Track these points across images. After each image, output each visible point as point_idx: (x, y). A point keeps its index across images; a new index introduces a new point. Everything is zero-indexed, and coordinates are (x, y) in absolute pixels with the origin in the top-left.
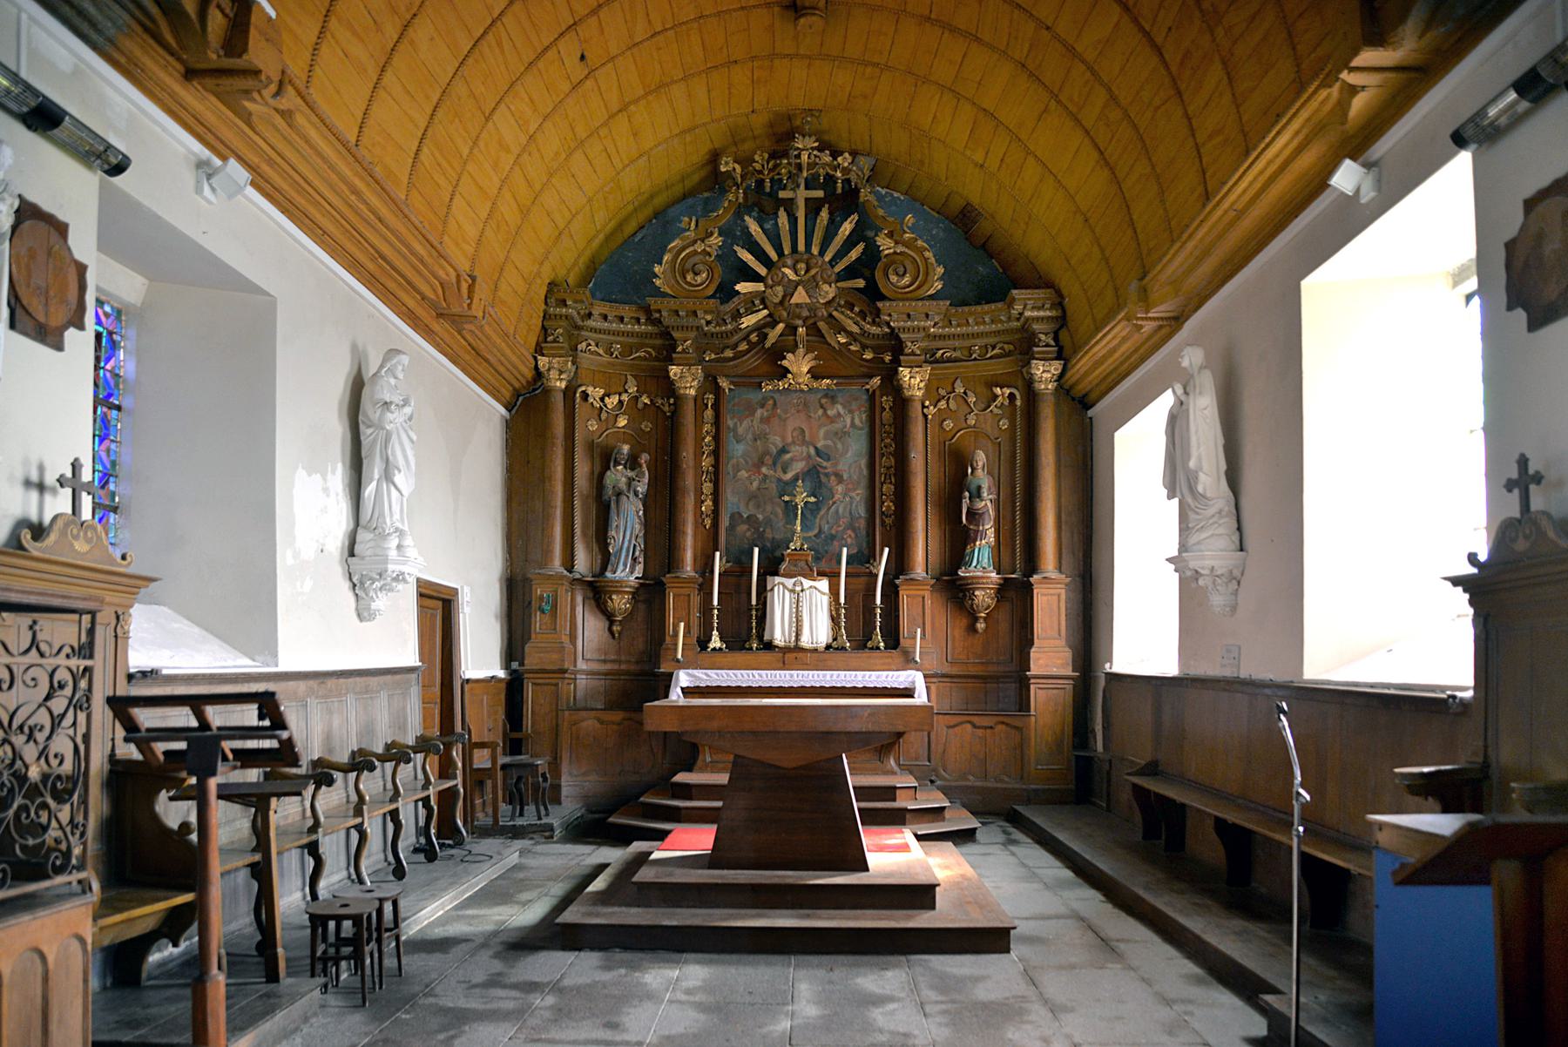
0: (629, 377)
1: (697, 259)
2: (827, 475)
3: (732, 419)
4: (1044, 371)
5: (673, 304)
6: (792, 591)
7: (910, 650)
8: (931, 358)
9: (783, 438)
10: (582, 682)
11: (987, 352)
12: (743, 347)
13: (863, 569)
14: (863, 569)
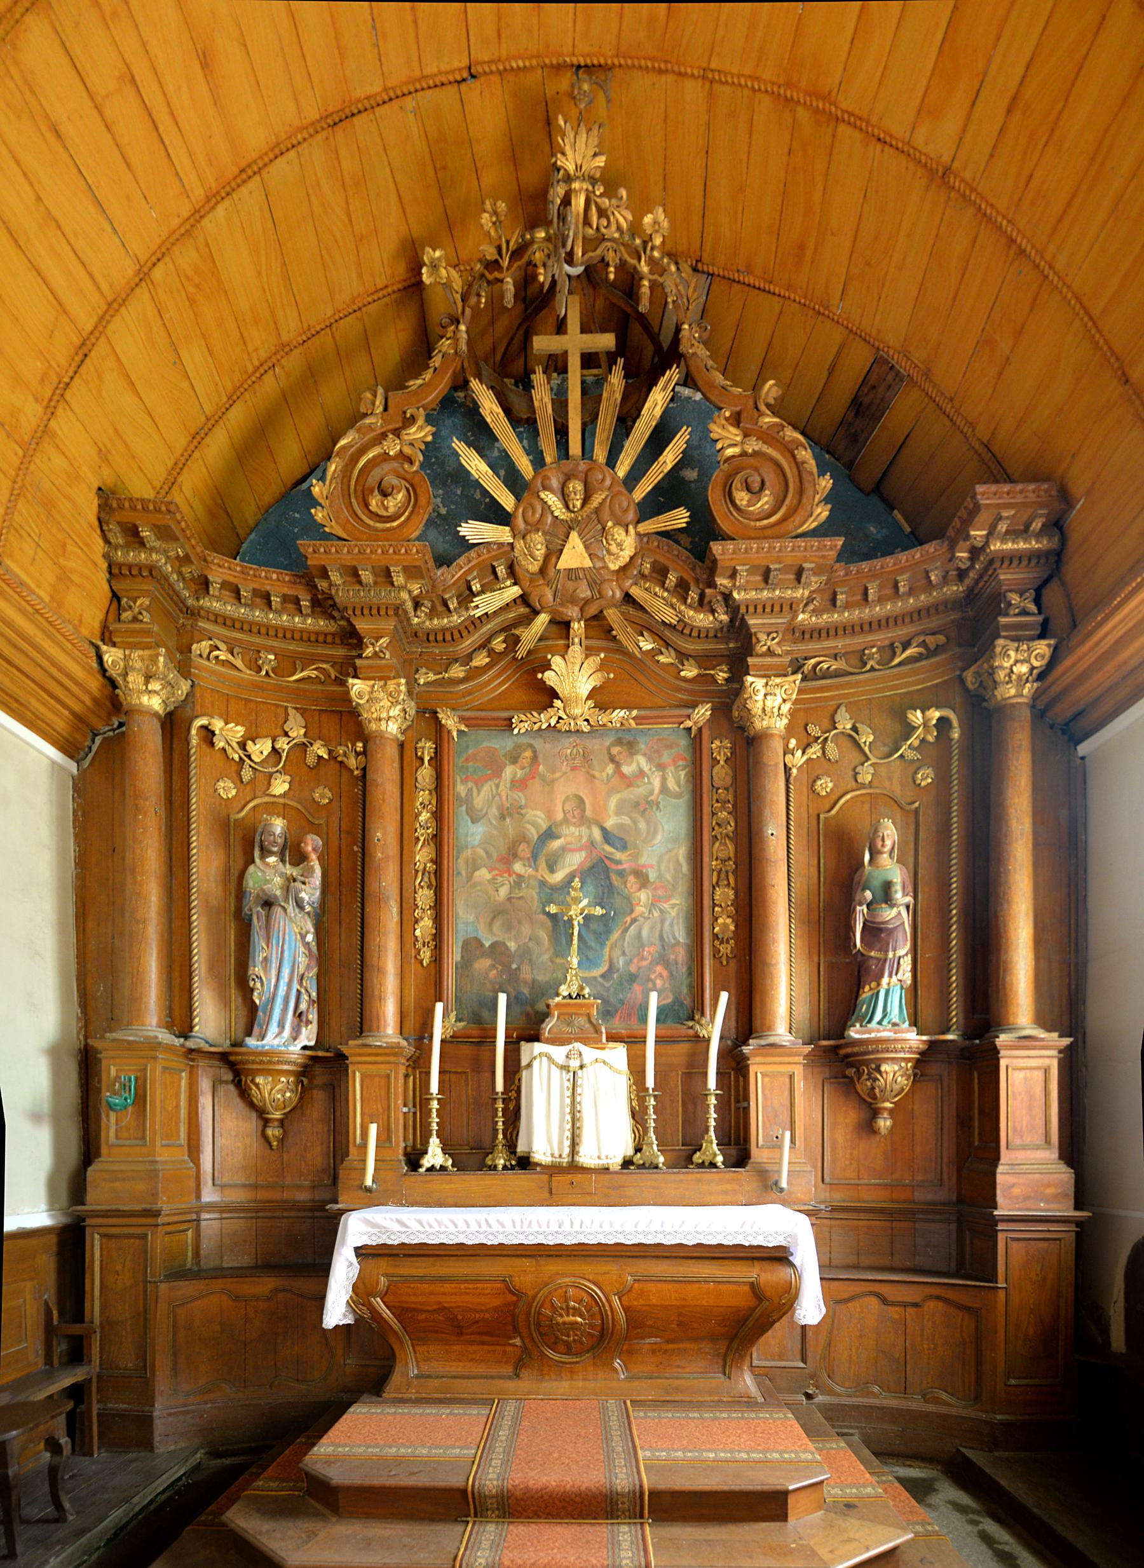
0: (291, 711)
1: (387, 467)
2: (621, 874)
3: (465, 781)
4: (1016, 662)
5: (345, 554)
6: (565, 1068)
7: (769, 1167)
9: (549, 814)
10: (210, 1224)
12: (481, 660)
13: (683, 1030)
14: (683, 1030)
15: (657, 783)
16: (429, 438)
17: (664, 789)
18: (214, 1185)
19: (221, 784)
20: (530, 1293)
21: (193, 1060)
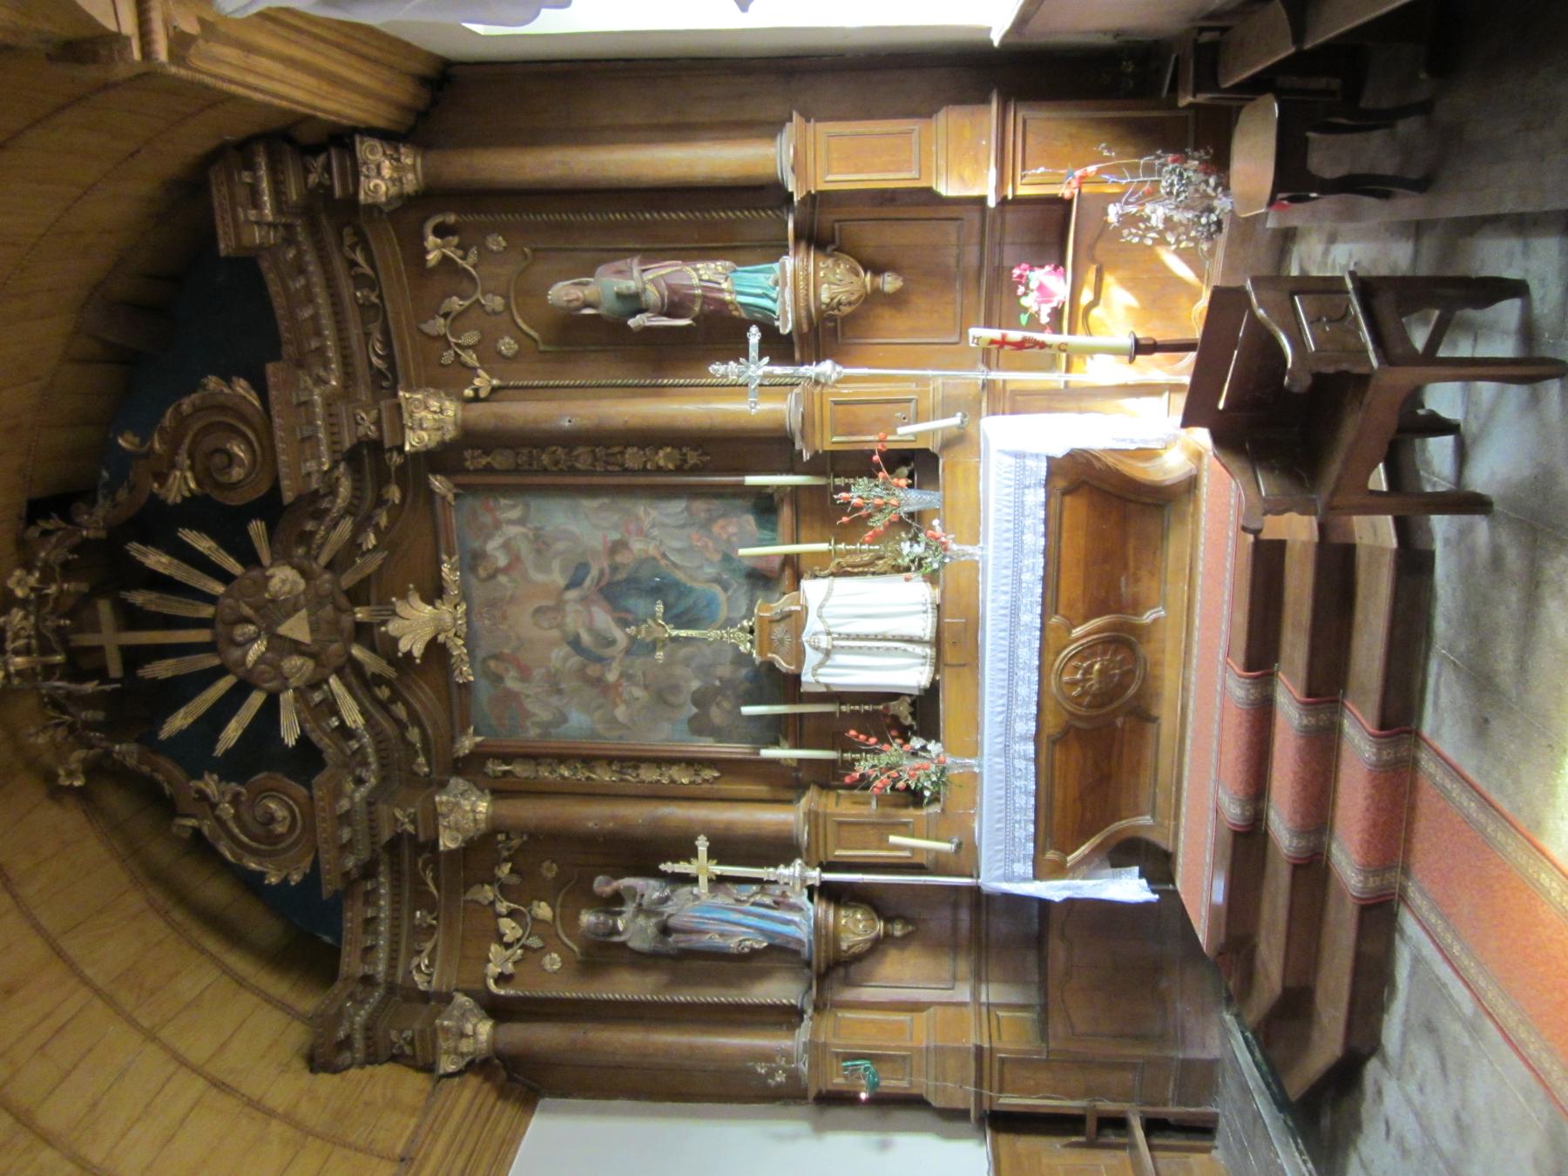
1: (246, 817)
2: (615, 568)
6: (828, 653)
8: (386, 381)
11: (364, 275)
15: (513, 530)
16: (216, 777)
17: (521, 522)
18: (952, 989)
19: (548, 967)
20: (1066, 716)
21: (825, 1005)
